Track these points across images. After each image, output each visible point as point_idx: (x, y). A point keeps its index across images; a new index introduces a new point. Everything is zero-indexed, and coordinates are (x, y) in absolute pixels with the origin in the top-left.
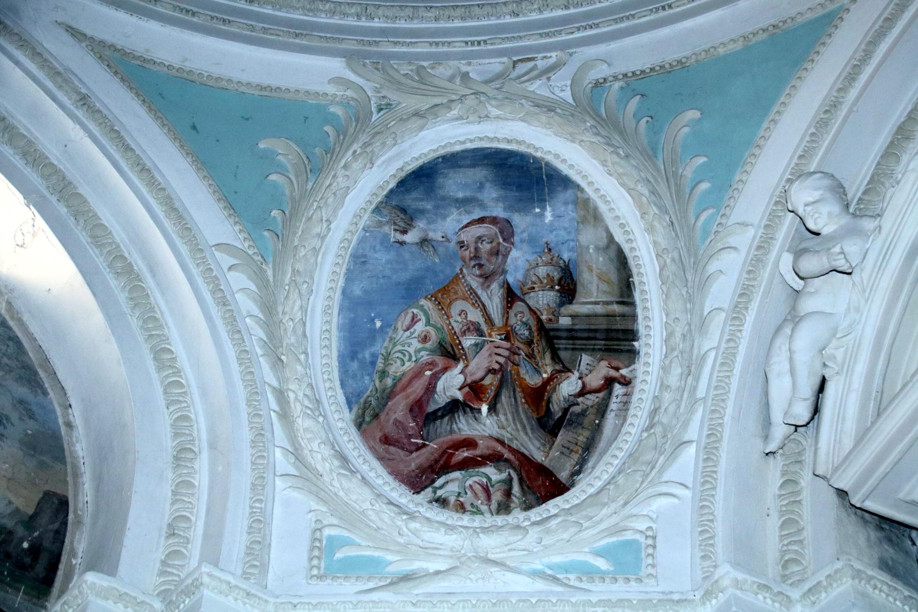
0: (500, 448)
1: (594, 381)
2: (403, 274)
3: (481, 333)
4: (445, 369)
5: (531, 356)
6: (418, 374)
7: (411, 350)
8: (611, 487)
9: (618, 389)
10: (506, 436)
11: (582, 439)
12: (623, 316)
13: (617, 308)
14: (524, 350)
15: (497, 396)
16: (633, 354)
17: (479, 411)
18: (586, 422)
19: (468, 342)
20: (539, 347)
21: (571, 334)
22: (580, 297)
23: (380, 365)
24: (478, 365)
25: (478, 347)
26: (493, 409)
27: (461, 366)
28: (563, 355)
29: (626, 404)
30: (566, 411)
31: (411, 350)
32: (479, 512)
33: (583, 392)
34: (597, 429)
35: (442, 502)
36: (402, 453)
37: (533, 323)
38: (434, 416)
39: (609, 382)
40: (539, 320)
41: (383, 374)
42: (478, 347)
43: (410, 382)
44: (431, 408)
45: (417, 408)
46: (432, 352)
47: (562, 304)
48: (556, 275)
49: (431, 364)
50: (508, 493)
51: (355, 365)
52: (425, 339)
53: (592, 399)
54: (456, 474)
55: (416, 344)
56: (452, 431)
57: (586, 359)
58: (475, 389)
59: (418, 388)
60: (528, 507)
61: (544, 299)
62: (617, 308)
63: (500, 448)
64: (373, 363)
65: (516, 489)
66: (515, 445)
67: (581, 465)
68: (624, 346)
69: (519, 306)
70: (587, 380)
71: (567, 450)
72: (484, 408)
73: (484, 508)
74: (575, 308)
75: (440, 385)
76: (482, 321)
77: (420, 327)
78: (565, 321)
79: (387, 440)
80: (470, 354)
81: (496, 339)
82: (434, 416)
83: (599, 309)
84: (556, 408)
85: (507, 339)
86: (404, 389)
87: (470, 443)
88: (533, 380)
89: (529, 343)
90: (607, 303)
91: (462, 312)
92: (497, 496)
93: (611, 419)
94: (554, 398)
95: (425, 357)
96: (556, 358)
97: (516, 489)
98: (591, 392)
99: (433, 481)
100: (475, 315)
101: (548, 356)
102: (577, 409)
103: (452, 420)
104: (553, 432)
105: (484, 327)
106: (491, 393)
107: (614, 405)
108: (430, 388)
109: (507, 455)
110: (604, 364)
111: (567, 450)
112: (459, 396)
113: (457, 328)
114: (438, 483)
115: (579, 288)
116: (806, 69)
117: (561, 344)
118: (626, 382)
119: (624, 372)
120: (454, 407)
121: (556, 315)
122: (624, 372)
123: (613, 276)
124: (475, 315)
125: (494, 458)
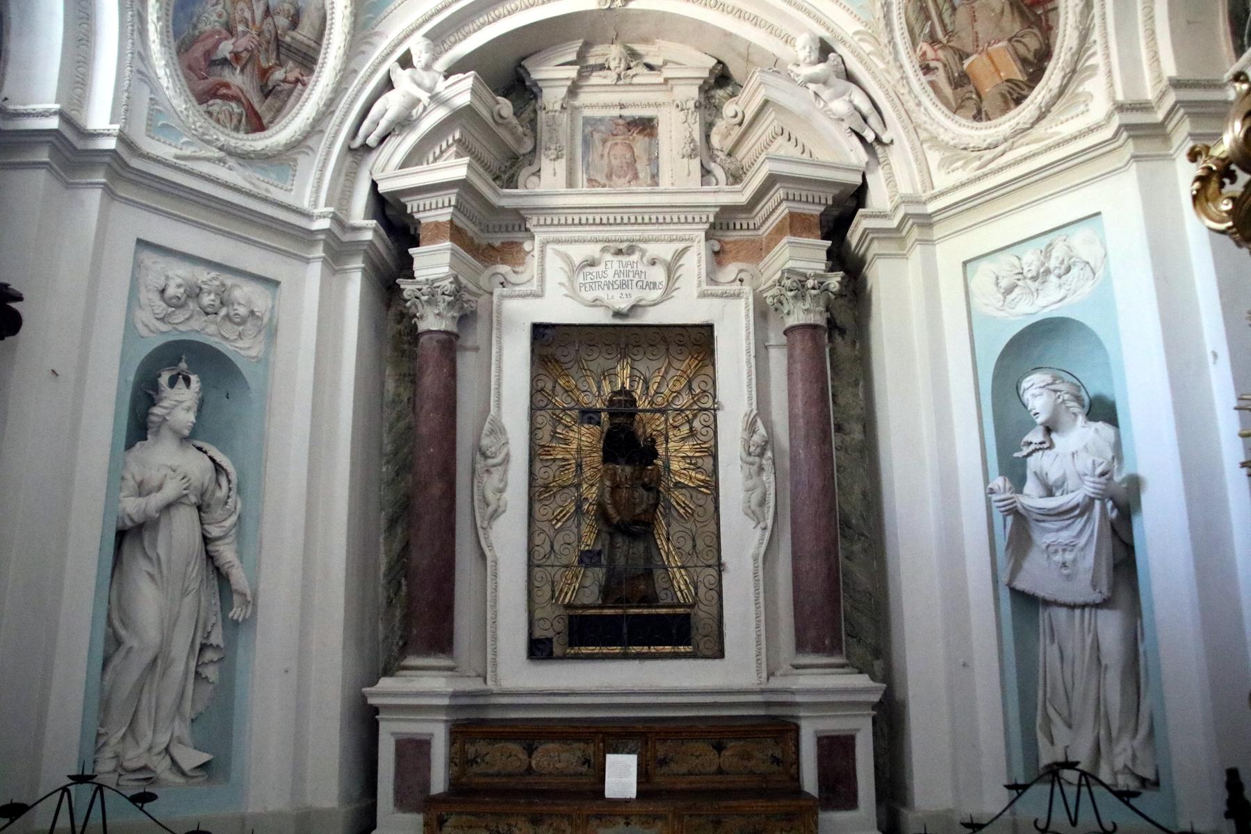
0: (241, 94)
1: (291, 77)
2: (564, 756)
3: (247, 26)
4: (226, 39)
5: (267, 50)
6: (211, 35)
7: (212, 19)
8: (713, 561)
9: (300, 86)
10: (244, 87)
11: (277, 105)
12: (314, 49)
13: (313, 44)
14: (265, 45)
15: (245, 65)
16: (311, 71)
17: (235, 69)
18: (281, 96)
19: (240, 28)
20: (273, 46)
21: (289, 47)
22: (299, 30)
23: (195, 19)
24: (243, 43)
25: (245, 33)
26: (242, 70)
27: (233, 40)
28: (282, 57)
29: (301, 95)
30: (274, 87)
31: (212, 19)
32: (226, 127)
33: (285, 81)
34: (285, 103)
35: (210, 114)
36: (196, 78)
37: (273, 33)
38: (213, 63)
39: (297, 81)
40: (277, 33)
41: (195, 27)
42: (245, 33)
43: (207, 37)
44: (214, 58)
45: (208, 54)
46: (222, 25)
47: (289, 29)
48: (292, 12)
49: (219, 32)
50: (240, 121)
51: (181, 15)
52: (220, 16)
53: (287, 86)
54: (219, 101)
55: (214, 18)
56: (221, 75)
57: (291, 64)
58: (237, 56)
59: (209, 43)
60: (247, 133)
61: (282, 22)
62: (313, 44)
63: (241, 94)
64: (191, 18)
65: (244, 119)
66: (248, 96)
67: (274, 118)
68: (309, 65)
69: (269, 20)
70: (288, 75)
71: (269, 109)
72: (239, 68)
73: (228, 125)
74: (293, 34)
75: (221, 47)
76: (250, 19)
77: (219, 8)
78: (288, 39)
79: (190, 68)
80: (240, 34)
81: (254, 32)
82: (213, 63)
83: (306, 41)
84: (270, 84)
85: (259, 35)
86: (203, 41)
87: (227, 86)
88: (265, 65)
89: (268, 43)
90: (309, 39)
91: (242, 10)
92: (235, 121)
93: (292, 99)
94: (271, 78)
95: (218, 26)
96: (278, 57)
97: (244, 119)
98: (289, 82)
99: (208, 101)
100: (247, 14)
101: (275, 54)
102: (279, 88)
103: (222, 68)
104: (266, 96)
105: (250, 24)
106: (243, 62)
107: (295, 94)
108: (216, 46)
109: (243, 100)
110: (298, 70)
111: (269, 109)
112: (228, 56)
113: (237, 18)
114: (211, 102)
115: (300, 25)
116: (363, 52)
117: (283, 50)
118: (304, 85)
119: (305, 78)
120: (224, 62)
121: (285, 34)
122: (305, 78)
123: (317, 26)
124: (247, 14)
125: (236, 99)
